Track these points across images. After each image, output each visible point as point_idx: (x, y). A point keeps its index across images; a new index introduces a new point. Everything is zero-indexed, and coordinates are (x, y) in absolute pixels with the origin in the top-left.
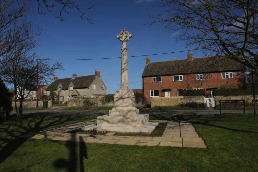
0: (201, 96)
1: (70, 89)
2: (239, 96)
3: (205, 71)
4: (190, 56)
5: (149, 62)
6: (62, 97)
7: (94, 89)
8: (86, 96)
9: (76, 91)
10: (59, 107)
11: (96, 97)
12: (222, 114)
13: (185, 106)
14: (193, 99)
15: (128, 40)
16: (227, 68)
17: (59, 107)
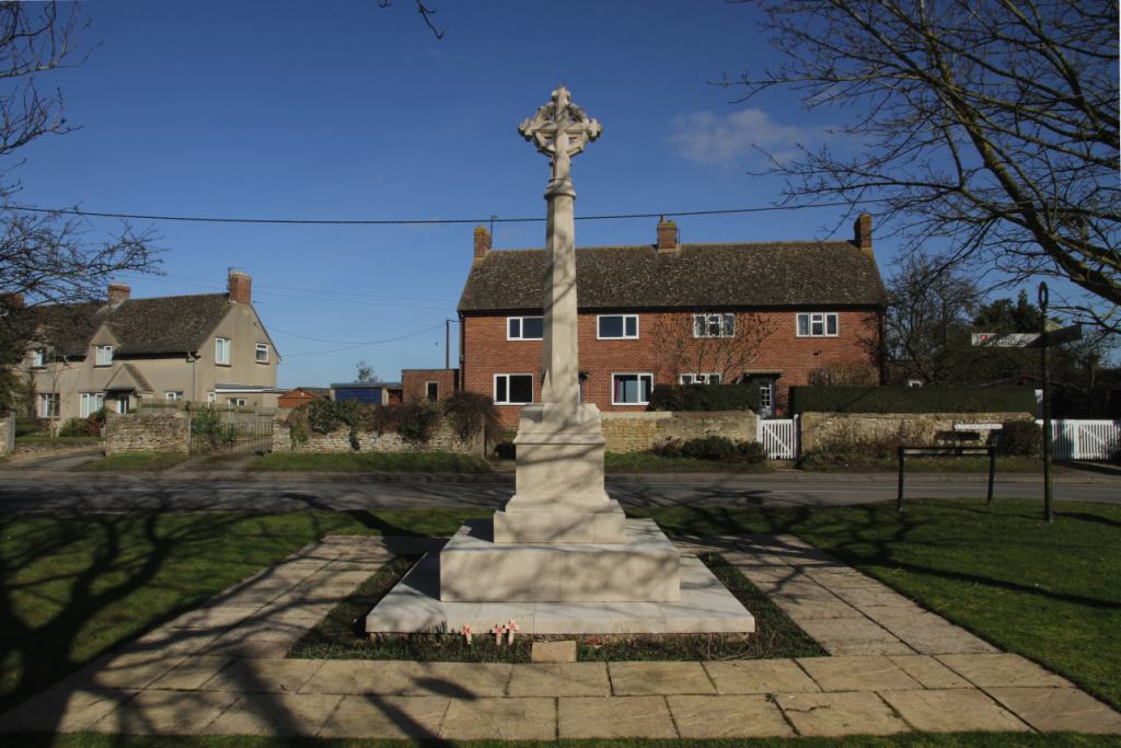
0: (743, 410)
1: (93, 358)
2: (892, 415)
3: (733, 301)
4: (667, 233)
5: (489, 248)
6: (50, 395)
7: (223, 362)
8: (179, 393)
9: (131, 369)
10: (52, 454)
11: (234, 401)
12: (909, 502)
13: (683, 456)
14: (710, 424)
15: (581, 152)
16: (817, 294)
17: (52, 454)
